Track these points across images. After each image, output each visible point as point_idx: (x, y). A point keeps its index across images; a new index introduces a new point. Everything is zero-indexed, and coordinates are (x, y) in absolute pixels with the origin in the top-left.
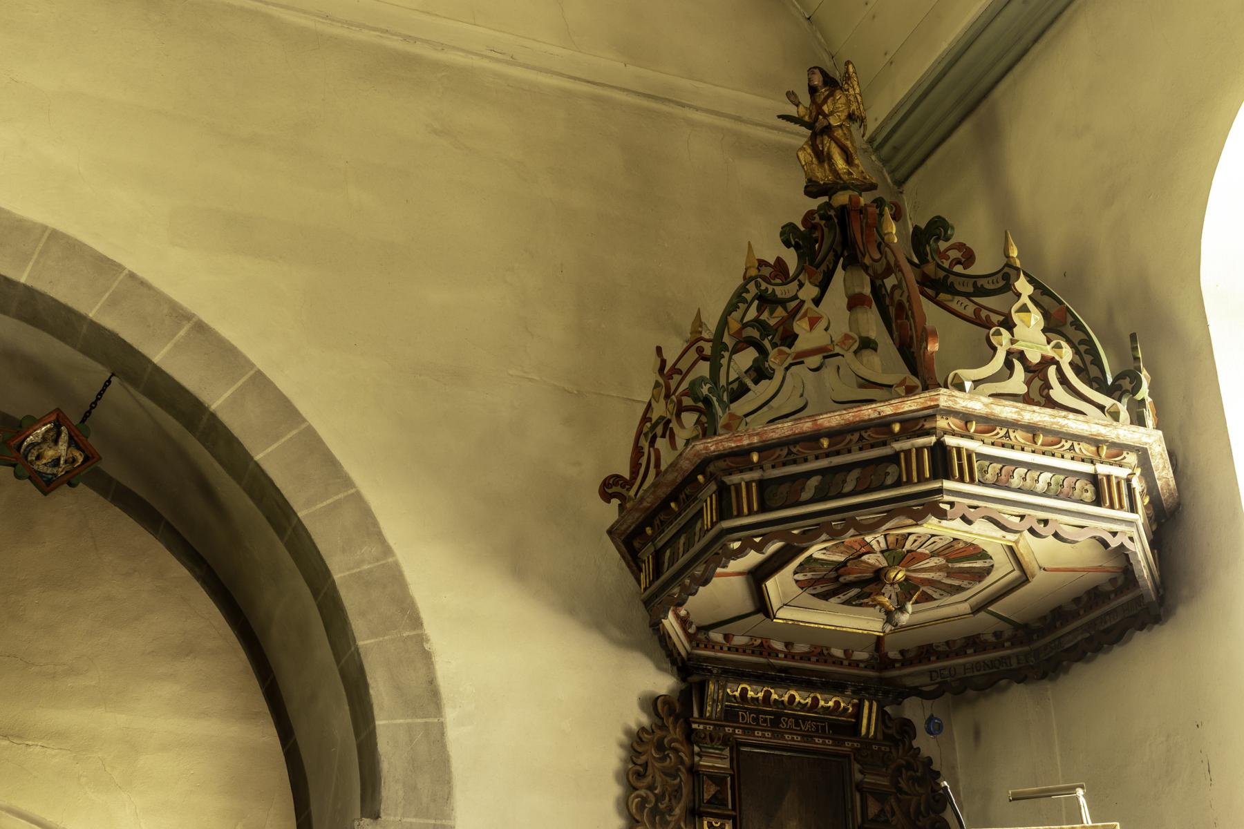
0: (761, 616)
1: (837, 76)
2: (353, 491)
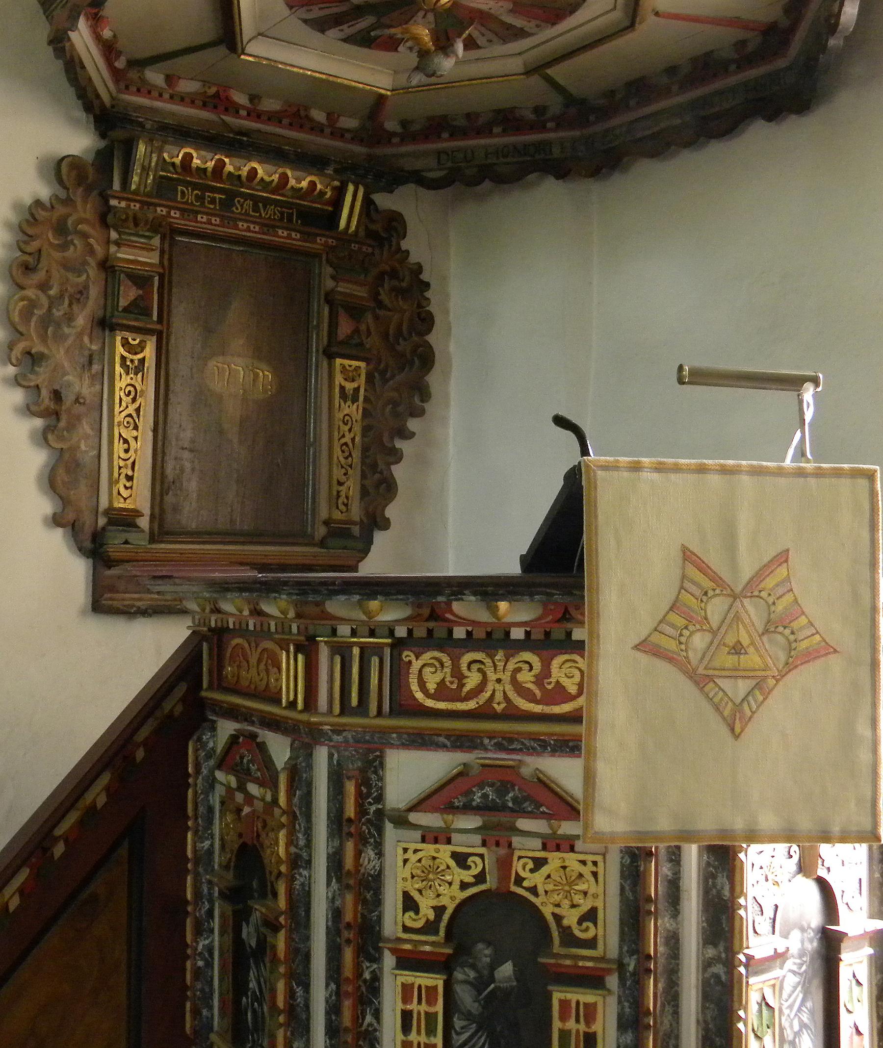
0: (222, 50)
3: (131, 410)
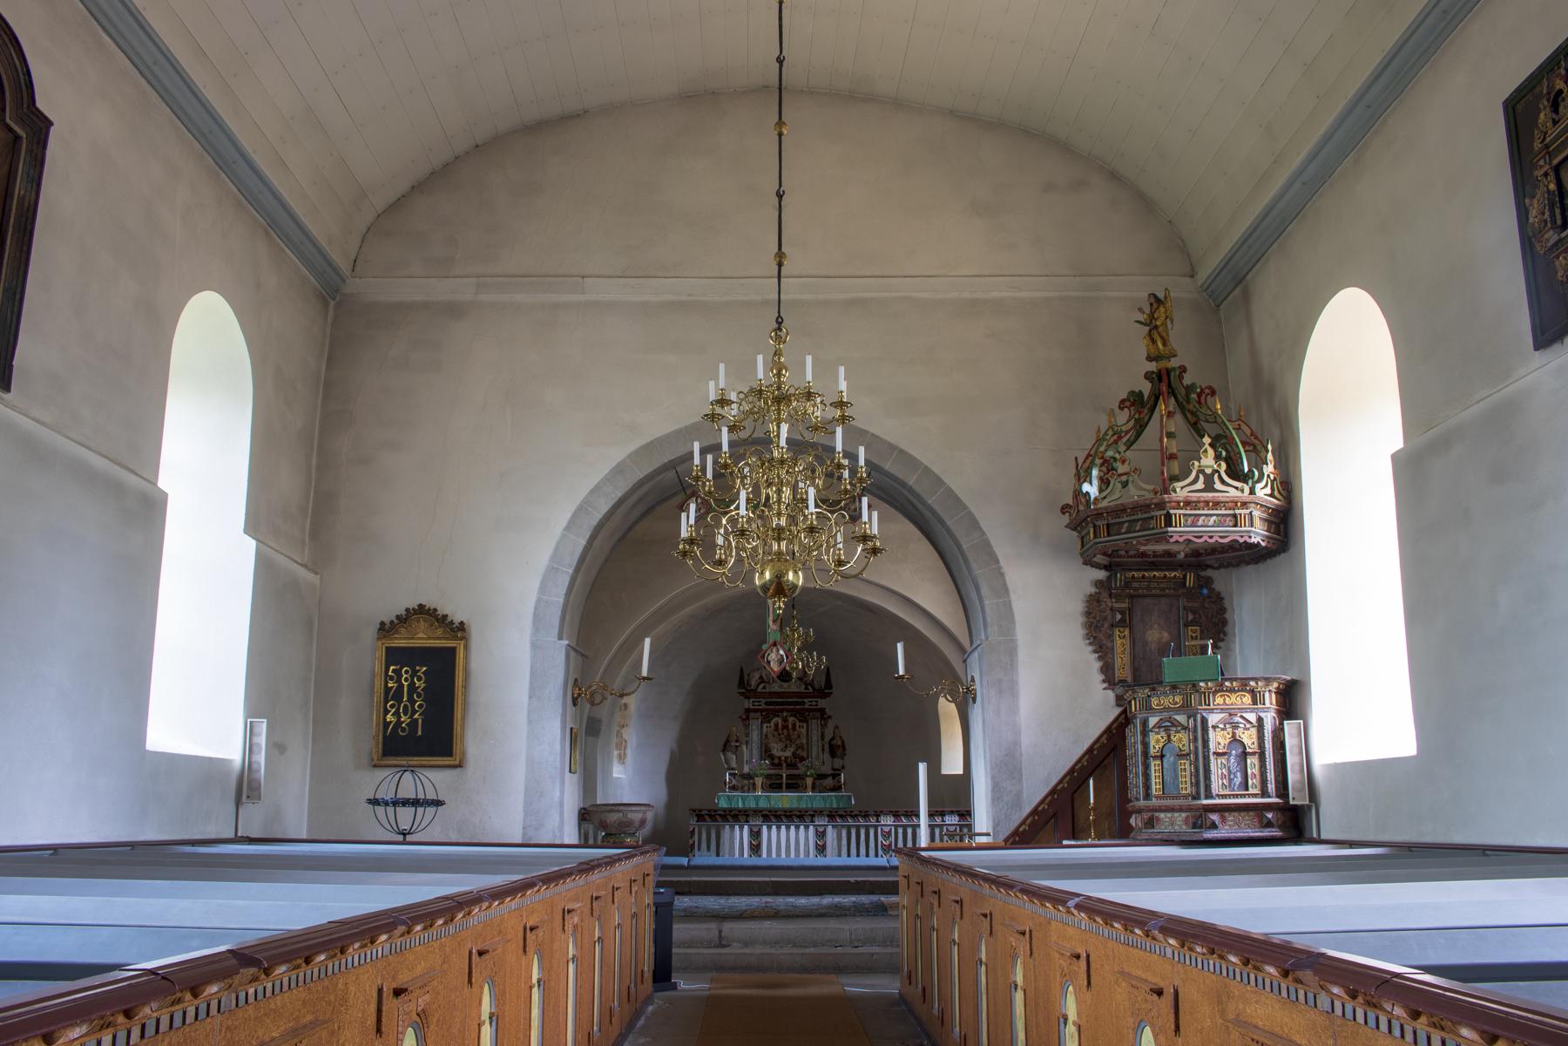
1: (1161, 296)
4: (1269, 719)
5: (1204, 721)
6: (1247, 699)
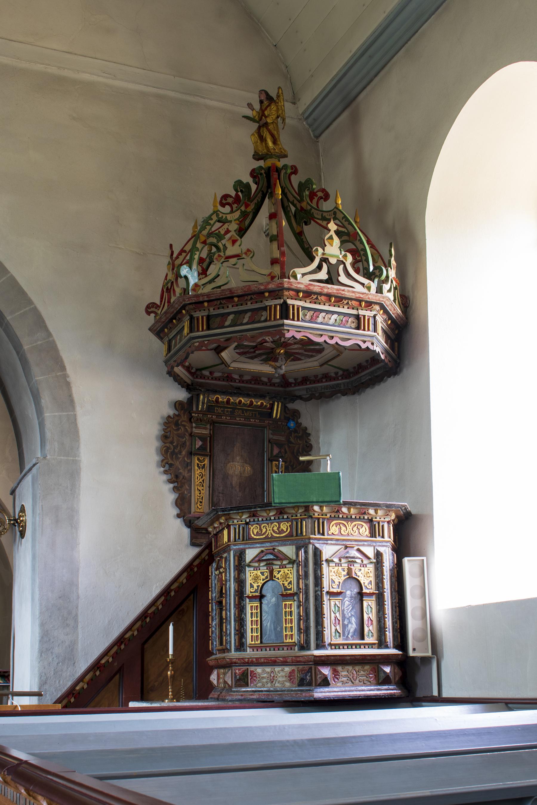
1: (273, 94)
2: (33, 306)
3: (201, 480)
4: (388, 559)
5: (317, 553)
6: (365, 529)
